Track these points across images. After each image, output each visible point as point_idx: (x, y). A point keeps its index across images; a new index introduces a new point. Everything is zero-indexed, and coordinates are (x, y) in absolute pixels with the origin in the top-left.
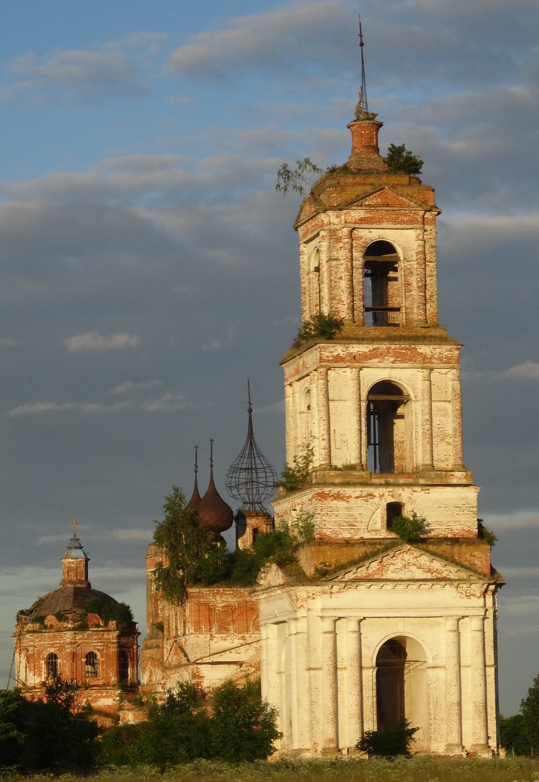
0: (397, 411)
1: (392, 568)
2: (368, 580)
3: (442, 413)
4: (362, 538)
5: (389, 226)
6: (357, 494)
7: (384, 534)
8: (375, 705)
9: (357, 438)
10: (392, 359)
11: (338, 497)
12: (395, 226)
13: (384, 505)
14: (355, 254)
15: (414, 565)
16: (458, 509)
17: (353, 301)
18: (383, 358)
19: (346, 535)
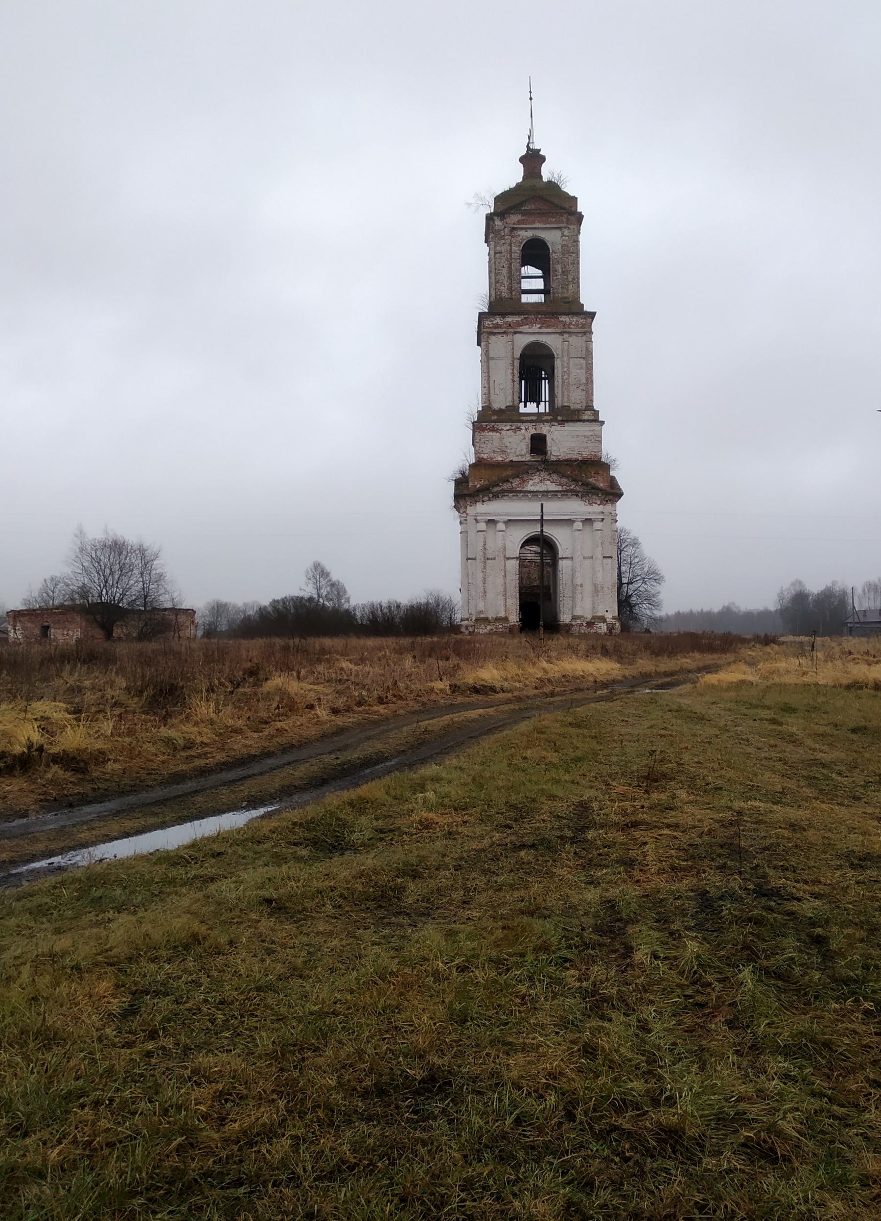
0: (541, 177)
1: (531, 482)
2: (511, 491)
3: (578, 367)
4: (511, 461)
5: (540, 226)
6: (508, 428)
7: (528, 458)
8: (518, 586)
9: (510, 386)
10: (539, 326)
11: (493, 430)
12: (549, 330)
13: (528, 436)
14: (514, 248)
15: (549, 480)
16: (587, 439)
17: (511, 284)
18: (532, 326)
19: (499, 458)
